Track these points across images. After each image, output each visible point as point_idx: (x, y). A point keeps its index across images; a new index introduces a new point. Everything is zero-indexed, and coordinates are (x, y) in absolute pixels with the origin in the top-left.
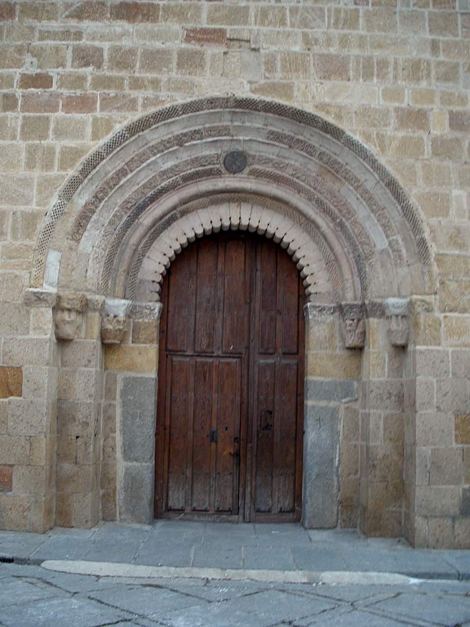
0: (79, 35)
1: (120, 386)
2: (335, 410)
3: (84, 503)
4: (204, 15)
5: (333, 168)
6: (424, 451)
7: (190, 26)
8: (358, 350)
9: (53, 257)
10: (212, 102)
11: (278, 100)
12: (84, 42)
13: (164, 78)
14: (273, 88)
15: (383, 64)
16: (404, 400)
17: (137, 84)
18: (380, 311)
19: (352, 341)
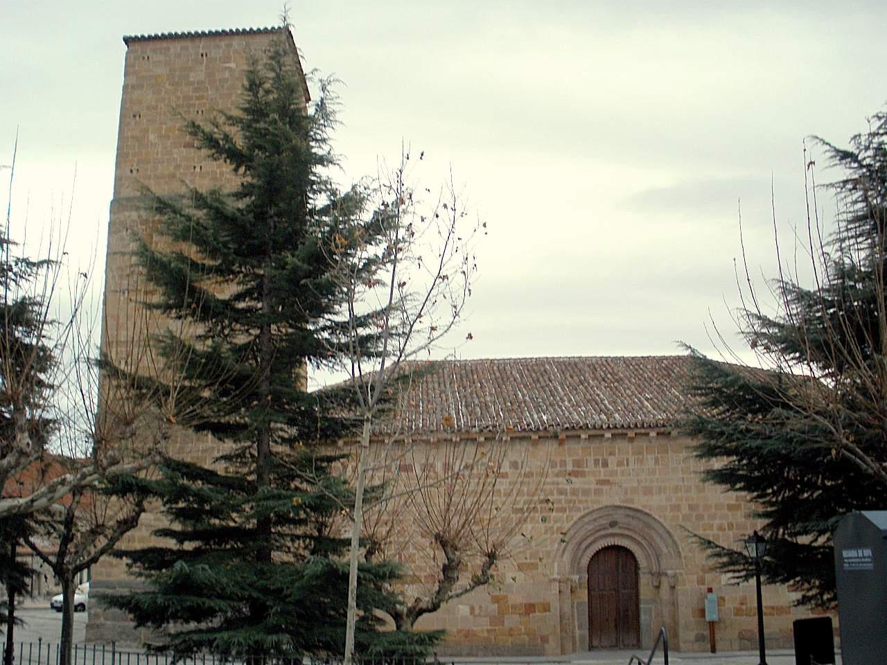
0: (558, 484)
1: (575, 604)
2: (650, 609)
3: (569, 646)
4: (602, 474)
5: (648, 526)
6: (682, 622)
7: (598, 478)
8: (658, 587)
9: (556, 564)
10: (606, 507)
11: (629, 505)
12: (560, 486)
13: (589, 499)
14: (626, 501)
15: (665, 488)
16: (674, 604)
17: (580, 502)
18: (666, 575)
19: (656, 584)
